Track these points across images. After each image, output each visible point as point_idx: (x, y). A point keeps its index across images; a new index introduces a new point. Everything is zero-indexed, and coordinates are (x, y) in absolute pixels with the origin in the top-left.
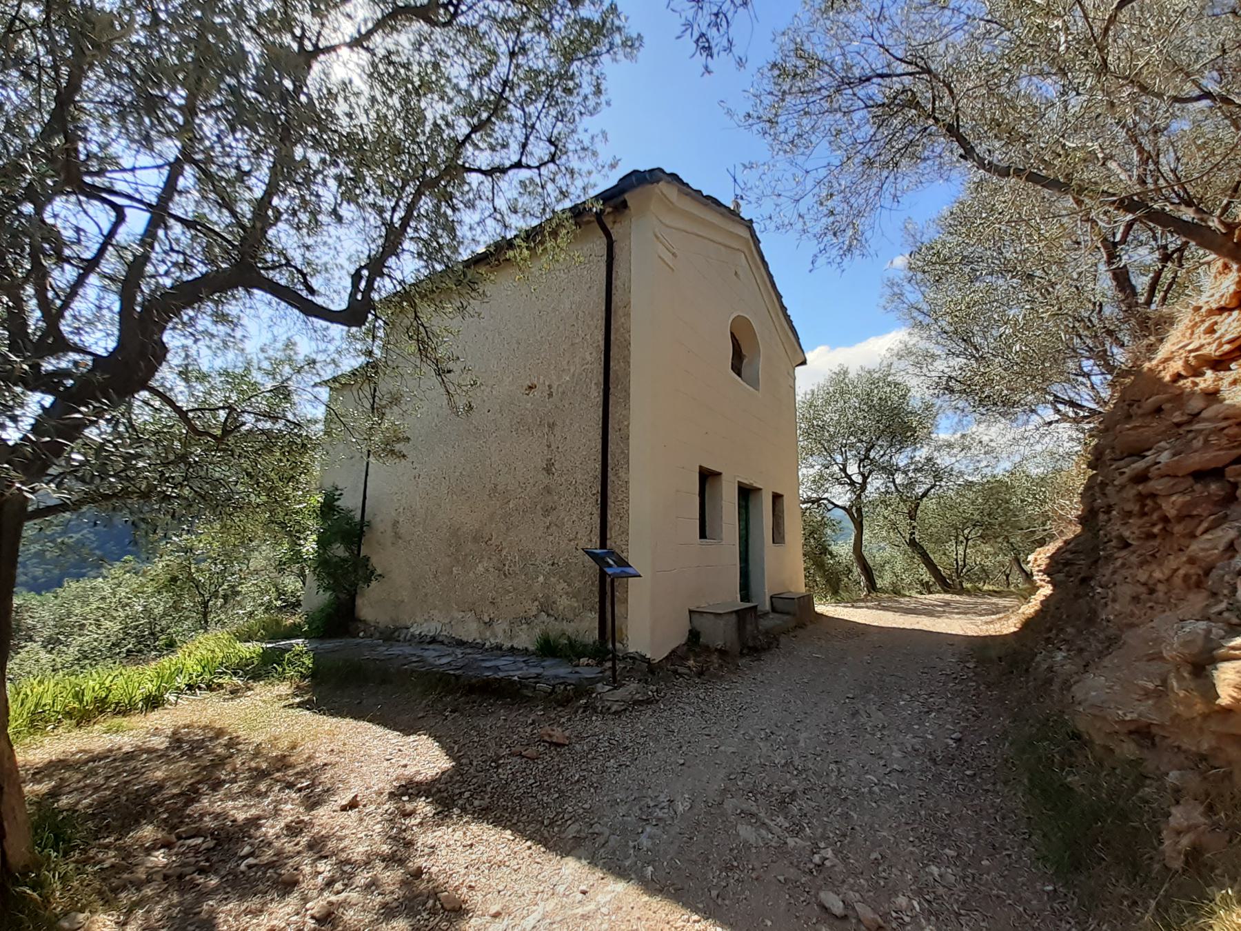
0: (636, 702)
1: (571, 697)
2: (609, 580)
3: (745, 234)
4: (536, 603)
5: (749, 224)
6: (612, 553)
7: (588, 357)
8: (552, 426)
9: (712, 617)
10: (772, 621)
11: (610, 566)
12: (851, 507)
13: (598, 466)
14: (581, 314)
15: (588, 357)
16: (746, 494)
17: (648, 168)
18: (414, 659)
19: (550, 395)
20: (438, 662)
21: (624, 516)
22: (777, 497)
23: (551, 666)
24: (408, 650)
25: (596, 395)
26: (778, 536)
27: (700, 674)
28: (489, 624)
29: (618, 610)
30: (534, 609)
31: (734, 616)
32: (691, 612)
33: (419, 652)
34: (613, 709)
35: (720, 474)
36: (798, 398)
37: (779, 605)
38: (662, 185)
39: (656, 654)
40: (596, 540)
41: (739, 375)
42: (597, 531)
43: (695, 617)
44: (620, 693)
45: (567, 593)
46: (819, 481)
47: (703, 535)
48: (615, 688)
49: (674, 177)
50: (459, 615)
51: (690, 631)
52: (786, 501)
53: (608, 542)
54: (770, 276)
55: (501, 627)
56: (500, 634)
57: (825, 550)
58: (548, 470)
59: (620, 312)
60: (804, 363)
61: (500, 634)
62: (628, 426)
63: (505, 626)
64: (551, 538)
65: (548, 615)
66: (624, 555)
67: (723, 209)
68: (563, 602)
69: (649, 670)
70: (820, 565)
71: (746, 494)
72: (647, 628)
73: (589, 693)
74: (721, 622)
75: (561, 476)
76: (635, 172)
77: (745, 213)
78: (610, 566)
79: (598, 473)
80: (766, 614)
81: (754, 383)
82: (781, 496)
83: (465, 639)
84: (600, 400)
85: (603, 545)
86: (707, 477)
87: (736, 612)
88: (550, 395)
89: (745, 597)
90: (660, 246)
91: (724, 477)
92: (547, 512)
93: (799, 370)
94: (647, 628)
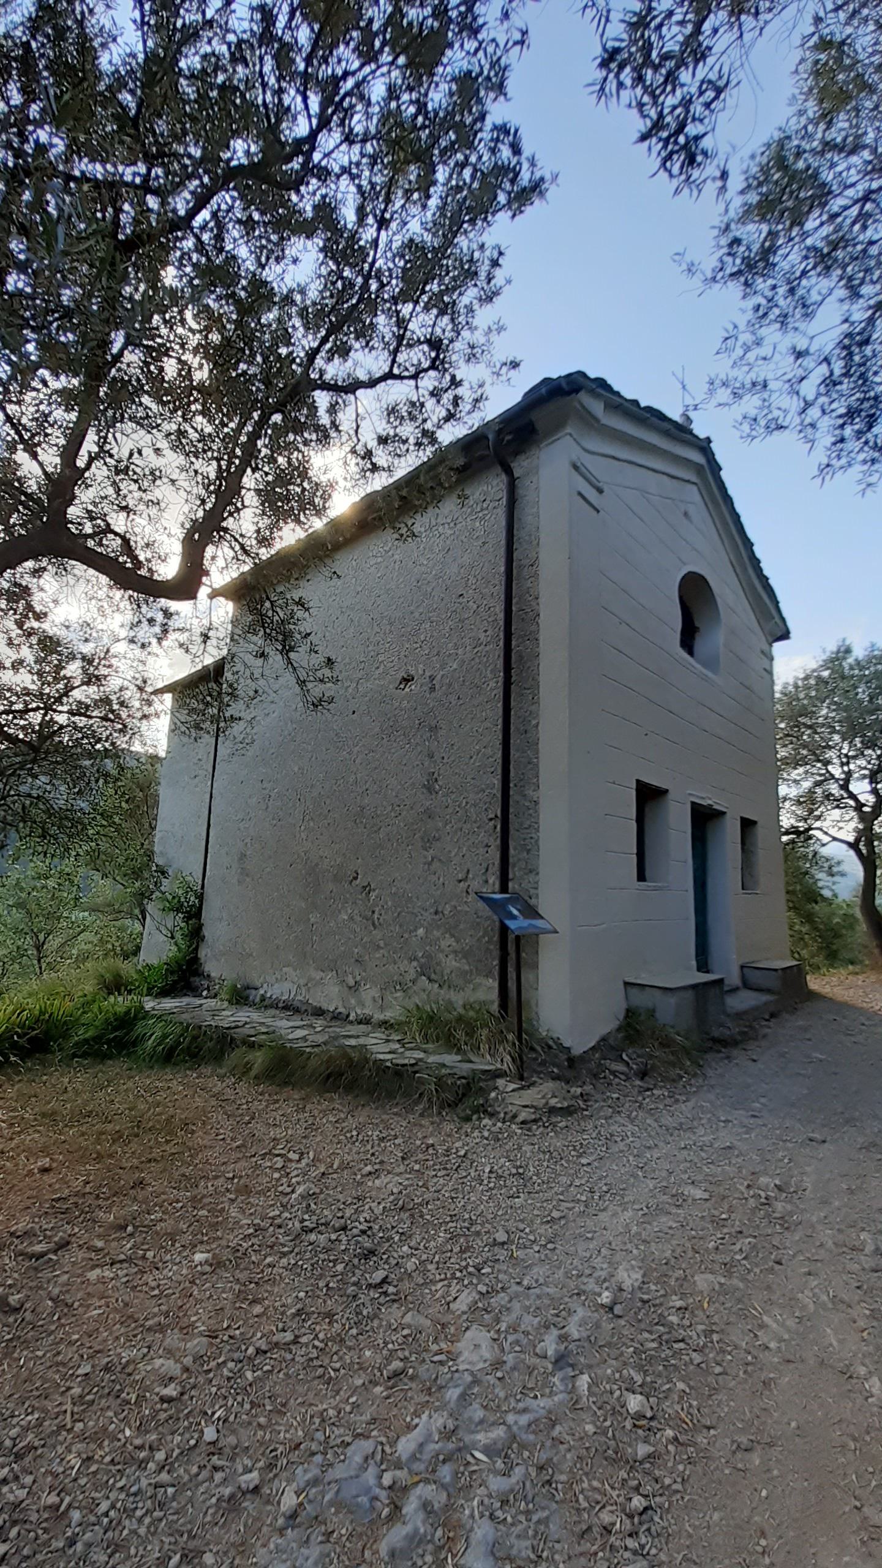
0: (553, 1111)
1: (465, 1098)
2: (511, 937)
3: (697, 457)
4: (415, 964)
5: (704, 447)
6: (516, 899)
7: (482, 636)
8: (434, 729)
9: (657, 993)
10: (743, 1001)
11: (514, 917)
12: (858, 840)
13: (497, 781)
14: (472, 580)
15: (482, 636)
16: (747, 825)
17: (563, 373)
18: (264, 1030)
19: (433, 689)
20: (290, 1037)
21: (531, 848)
22: (747, 825)
23: (434, 1053)
24: (255, 1016)
25: (495, 686)
26: (748, 880)
27: (643, 1075)
28: (355, 988)
29: (527, 976)
30: (412, 971)
31: (690, 994)
32: (626, 984)
33: (268, 1021)
34: (520, 1118)
35: (666, 792)
36: (778, 688)
37: (754, 977)
38: (584, 397)
39: (579, 1043)
40: (494, 880)
41: (691, 653)
42: (496, 868)
43: (633, 991)
44: (531, 1096)
45: (455, 952)
46: (809, 802)
47: (641, 877)
48: (522, 1088)
49: (602, 383)
50: (318, 975)
51: (628, 1011)
52: (761, 833)
53: (510, 884)
54: (736, 517)
55: (369, 993)
56: (369, 1002)
57: (813, 896)
58: (429, 789)
59: (525, 572)
60: (785, 635)
61: (369, 1002)
62: (537, 725)
63: (375, 992)
64: (434, 878)
65: (430, 980)
66: (533, 902)
67: (666, 425)
68: (451, 964)
69: (573, 1067)
70: (809, 918)
71: (704, 819)
72: (567, 1004)
73: (483, 1092)
74: (672, 1000)
75: (446, 795)
76: (546, 380)
77: (700, 430)
78: (514, 917)
79: (497, 792)
80: (734, 990)
81: (712, 664)
82: (754, 823)
83: (325, 1007)
84: (500, 692)
85: (504, 889)
86: (648, 796)
87: (694, 987)
88: (433, 689)
89: (703, 965)
90: (580, 479)
91: (671, 795)
92: (429, 841)
93: (778, 647)
94: (567, 1004)
